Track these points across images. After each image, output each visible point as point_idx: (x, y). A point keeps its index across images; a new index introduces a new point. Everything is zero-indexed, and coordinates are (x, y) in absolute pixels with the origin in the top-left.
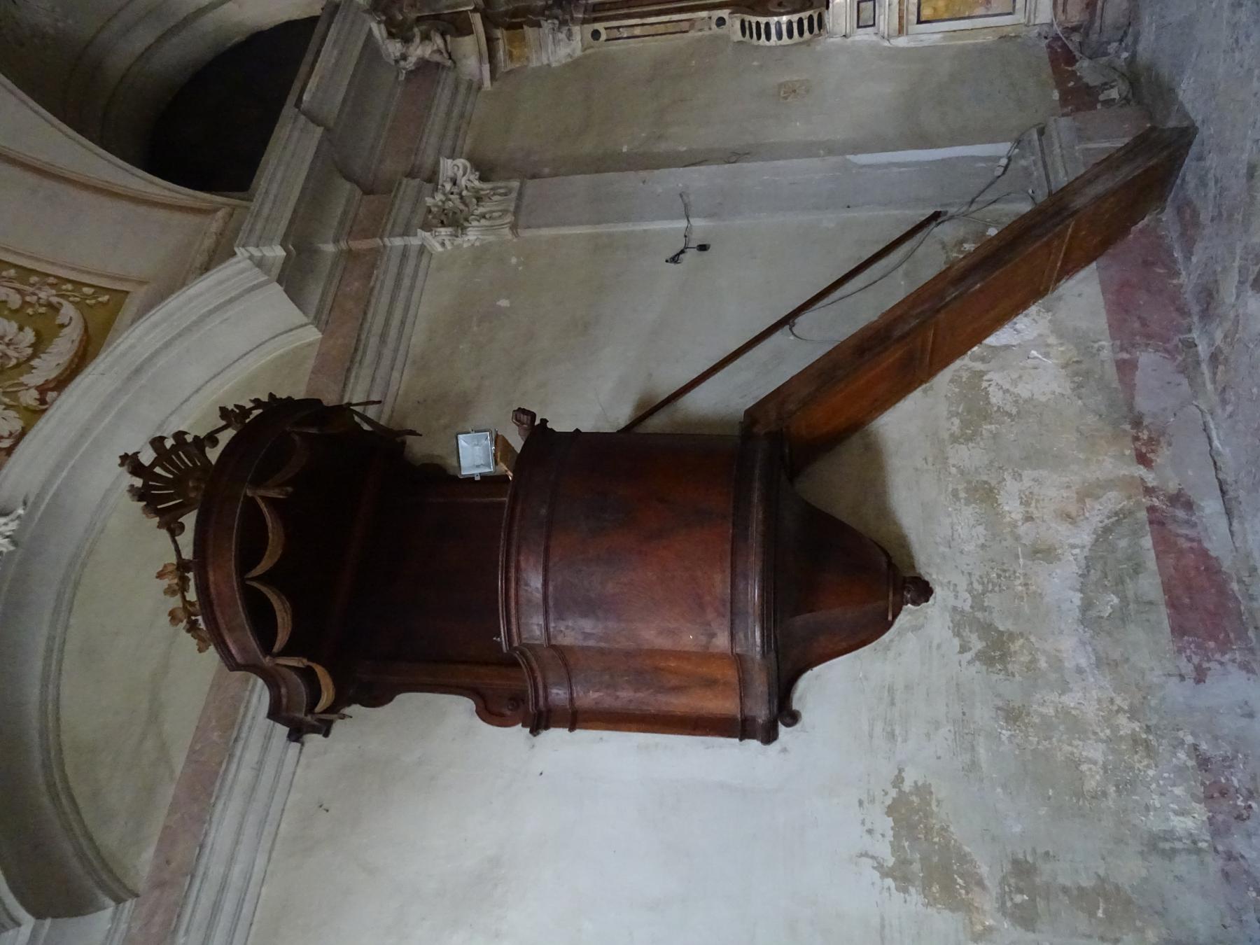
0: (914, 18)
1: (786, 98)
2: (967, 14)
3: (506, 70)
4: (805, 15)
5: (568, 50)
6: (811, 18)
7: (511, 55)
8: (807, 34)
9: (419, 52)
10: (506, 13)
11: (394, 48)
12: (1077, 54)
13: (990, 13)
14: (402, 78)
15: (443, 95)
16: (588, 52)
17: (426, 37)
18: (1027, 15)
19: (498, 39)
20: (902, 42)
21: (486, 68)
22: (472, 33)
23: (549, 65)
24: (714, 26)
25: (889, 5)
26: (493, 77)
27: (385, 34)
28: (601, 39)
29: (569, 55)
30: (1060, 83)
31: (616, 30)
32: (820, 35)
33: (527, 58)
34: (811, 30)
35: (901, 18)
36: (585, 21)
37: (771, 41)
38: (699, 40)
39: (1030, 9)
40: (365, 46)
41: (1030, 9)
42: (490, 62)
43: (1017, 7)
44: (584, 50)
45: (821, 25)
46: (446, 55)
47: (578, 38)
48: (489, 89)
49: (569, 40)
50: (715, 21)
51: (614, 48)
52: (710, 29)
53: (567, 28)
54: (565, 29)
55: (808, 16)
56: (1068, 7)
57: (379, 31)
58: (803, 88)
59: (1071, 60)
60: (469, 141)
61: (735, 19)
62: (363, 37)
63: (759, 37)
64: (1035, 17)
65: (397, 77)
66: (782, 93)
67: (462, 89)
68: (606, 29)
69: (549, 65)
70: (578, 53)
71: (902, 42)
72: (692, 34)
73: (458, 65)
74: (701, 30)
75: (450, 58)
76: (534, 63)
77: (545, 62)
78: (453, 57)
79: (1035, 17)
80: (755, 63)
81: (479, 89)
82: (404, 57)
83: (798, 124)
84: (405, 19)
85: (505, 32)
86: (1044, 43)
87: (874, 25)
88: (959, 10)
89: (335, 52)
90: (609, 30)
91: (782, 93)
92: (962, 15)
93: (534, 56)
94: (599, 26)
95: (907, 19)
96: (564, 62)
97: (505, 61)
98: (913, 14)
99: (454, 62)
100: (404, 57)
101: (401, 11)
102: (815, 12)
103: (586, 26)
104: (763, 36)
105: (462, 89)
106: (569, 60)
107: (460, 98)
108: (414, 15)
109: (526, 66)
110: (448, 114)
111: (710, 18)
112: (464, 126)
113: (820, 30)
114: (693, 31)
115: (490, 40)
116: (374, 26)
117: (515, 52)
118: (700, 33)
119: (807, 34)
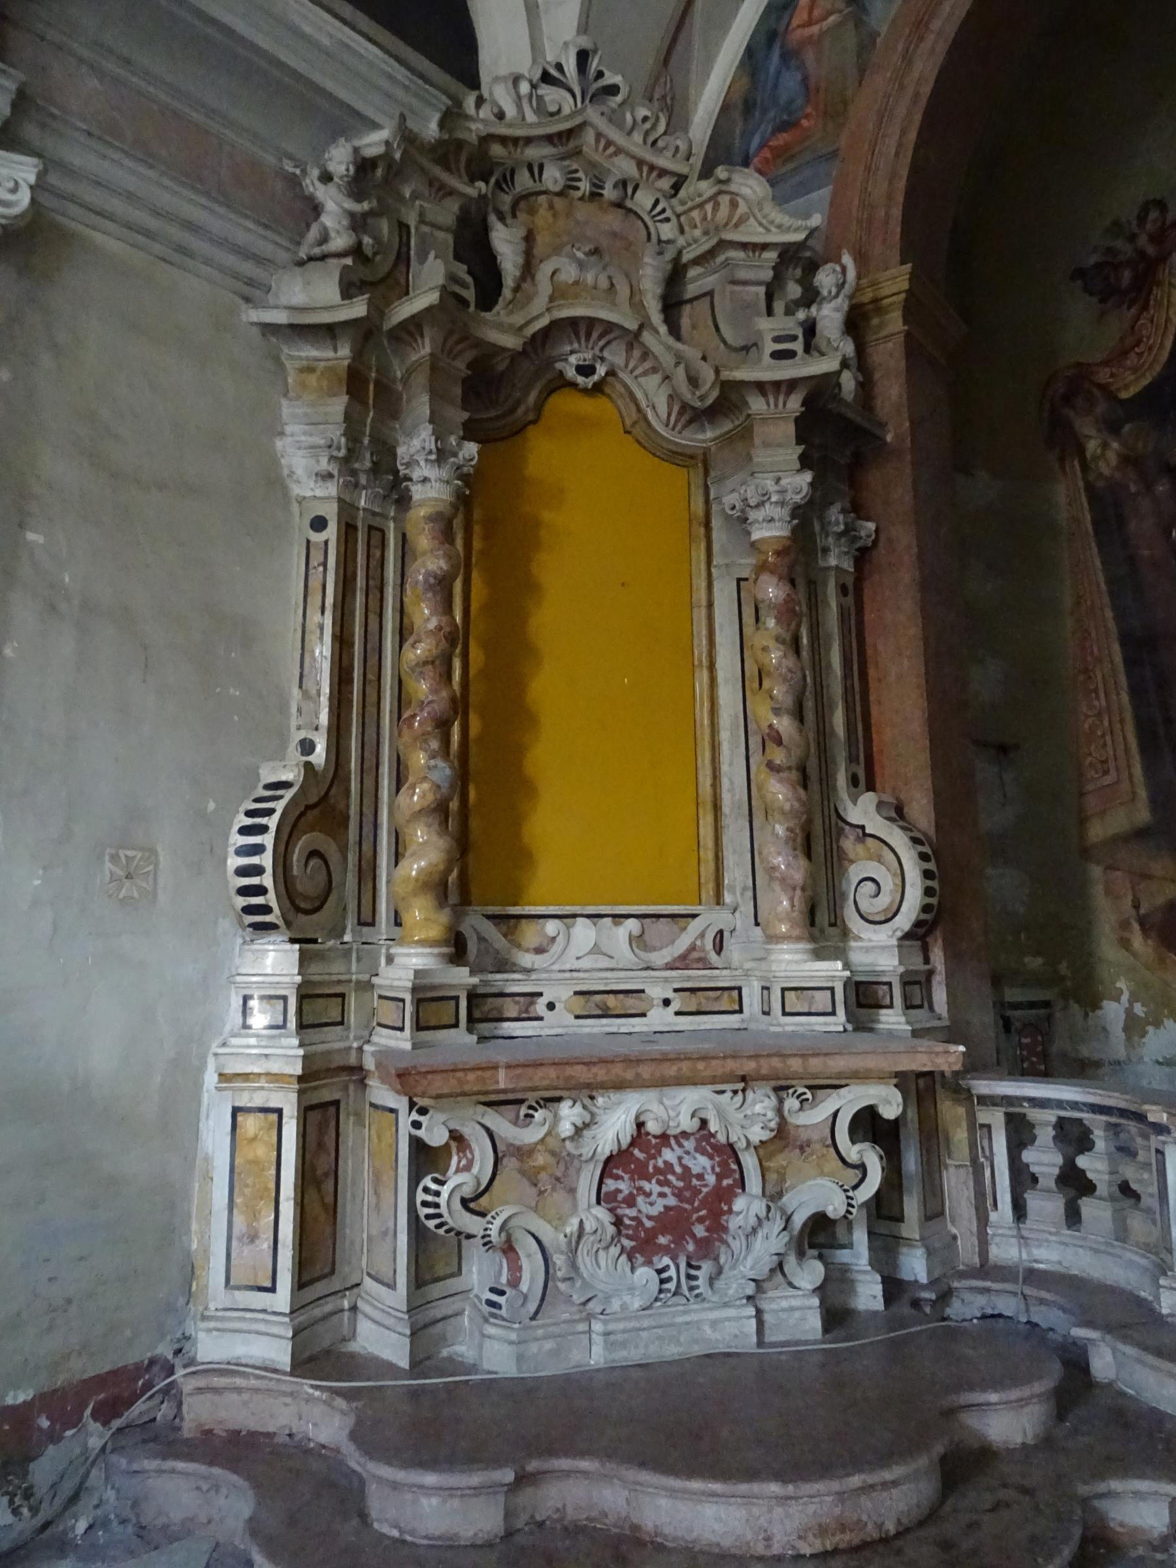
0: (244, 1101)
1: (115, 858)
2: (238, 1200)
3: (283, 358)
4: (271, 899)
5: (300, 472)
6: (266, 909)
7: (310, 370)
8: (242, 901)
9: (330, 206)
10: (384, 369)
11: (339, 159)
12: (116, 1423)
13: (234, 1243)
14: (289, 167)
15: (246, 233)
16: (295, 508)
17: (358, 223)
18: (219, 1314)
19: (335, 350)
20: (210, 1078)
21: (280, 317)
22: (343, 299)
23: (282, 434)
24: (302, 734)
25: (266, 1056)
26: (269, 329)
27: (370, 152)
28: (311, 532)
29: (292, 473)
30: (47, 1401)
31: (322, 559)
32: (243, 928)
33: (298, 398)
34: (249, 910)
35: (246, 1077)
36: (346, 508)
37: (238, 836)
38: (284, 708)
39: (230, 1319)
40: (357, 114)
41: (230, 1319)
42: (292, 326)
43: (237, 1293)
44: (301, 500)
45: (257, 927)
46: (317, 251)
47: (319, 493)
48: (244, 318)
49: (317, 475)
50: (309, 736)
51: (295, 552)
52: (299, 728)
53: (336, 473)
54: (334, 469)
55: (271, 904)
56: (209, 1395)
57: (374, 142)
58: (136, 894)
59: (105, 1413)
60: (113, 245)
61: (296, 771)
62: (370, 112)
63: (250, 814)
64: (209, 1331)
65: (291, 157)
66: (130, 853)
67: (248, 268)
68: (326, 542)
69: (282, 434)
70: (297, 490)
71: (210, 1078)
72: (296, 691)
73: (298, 270)
74: (299, 711)
75: (311, 259)
76: (287, 409)
77: (288, 429)
78: (313, 263)
79: (209, 1331)
80: (212, 806)
81: (247, 300)
82: (326, 178)
83: (37, 882)
84: (400, 198)
85: (346, 363)
86: (164, 1350)
87: (342, 1023)
88: (247, 1186)
89: (326, 41)
90: (323, 546)
91: (130, 853)
92: (236, 1190)
93: (300, 411)
94: (331, 532)
95: (243, 1089)
96: (283, 461)
97: (300, 358)
98: (251, 1099)
99: (301, 264)
100: (326, 178)
101: (415, 196)
102: (277, 917)
103: (335, 505)
104: (249, 821)
105: (248, 268)
106: (286, 472)
107: (231, 260)
108: (412, 220)
109: (285, 395)
110: (190, 226)
111: (317, 729)
112: (157, 248)
113: (251, 925)
114: (300, 696)
115: (329, 332)
116: (384, 134)
117: (312, 380)
118: (294, 710)
119: (242, 901)
